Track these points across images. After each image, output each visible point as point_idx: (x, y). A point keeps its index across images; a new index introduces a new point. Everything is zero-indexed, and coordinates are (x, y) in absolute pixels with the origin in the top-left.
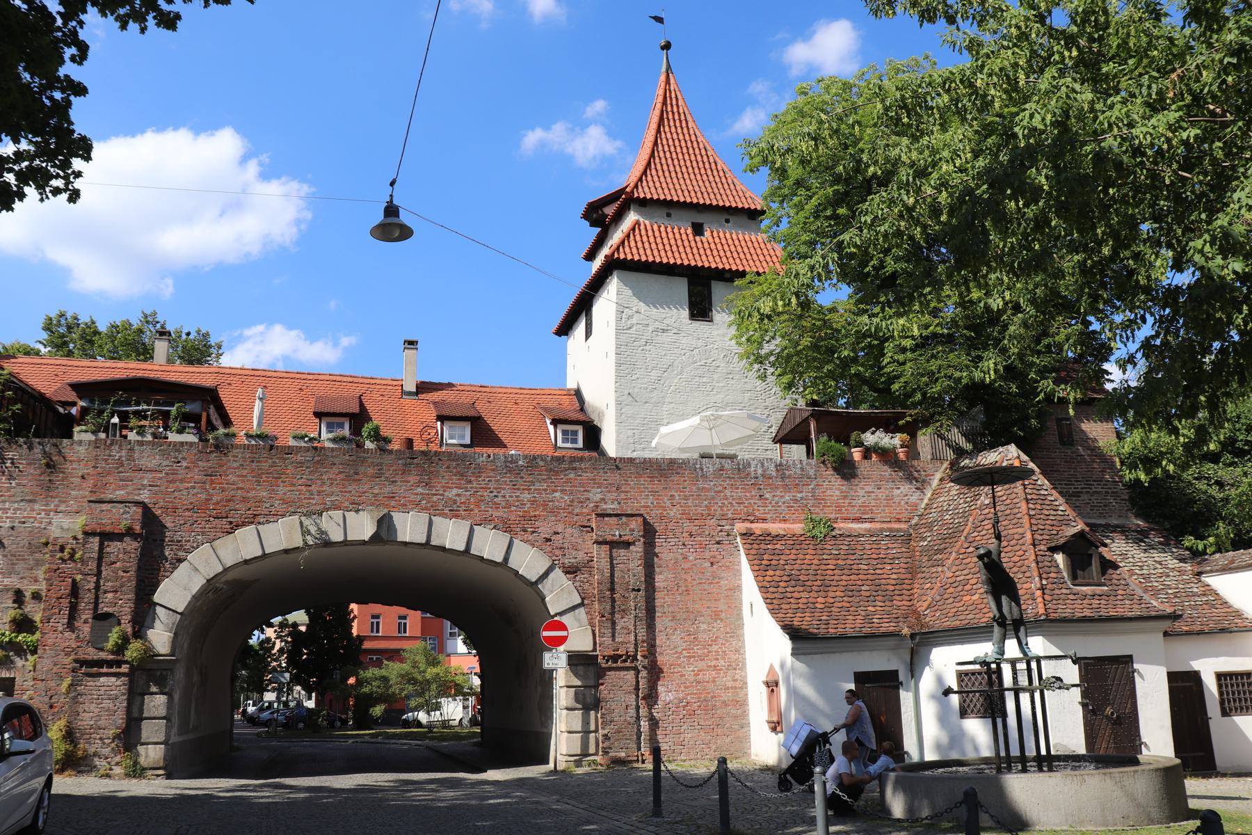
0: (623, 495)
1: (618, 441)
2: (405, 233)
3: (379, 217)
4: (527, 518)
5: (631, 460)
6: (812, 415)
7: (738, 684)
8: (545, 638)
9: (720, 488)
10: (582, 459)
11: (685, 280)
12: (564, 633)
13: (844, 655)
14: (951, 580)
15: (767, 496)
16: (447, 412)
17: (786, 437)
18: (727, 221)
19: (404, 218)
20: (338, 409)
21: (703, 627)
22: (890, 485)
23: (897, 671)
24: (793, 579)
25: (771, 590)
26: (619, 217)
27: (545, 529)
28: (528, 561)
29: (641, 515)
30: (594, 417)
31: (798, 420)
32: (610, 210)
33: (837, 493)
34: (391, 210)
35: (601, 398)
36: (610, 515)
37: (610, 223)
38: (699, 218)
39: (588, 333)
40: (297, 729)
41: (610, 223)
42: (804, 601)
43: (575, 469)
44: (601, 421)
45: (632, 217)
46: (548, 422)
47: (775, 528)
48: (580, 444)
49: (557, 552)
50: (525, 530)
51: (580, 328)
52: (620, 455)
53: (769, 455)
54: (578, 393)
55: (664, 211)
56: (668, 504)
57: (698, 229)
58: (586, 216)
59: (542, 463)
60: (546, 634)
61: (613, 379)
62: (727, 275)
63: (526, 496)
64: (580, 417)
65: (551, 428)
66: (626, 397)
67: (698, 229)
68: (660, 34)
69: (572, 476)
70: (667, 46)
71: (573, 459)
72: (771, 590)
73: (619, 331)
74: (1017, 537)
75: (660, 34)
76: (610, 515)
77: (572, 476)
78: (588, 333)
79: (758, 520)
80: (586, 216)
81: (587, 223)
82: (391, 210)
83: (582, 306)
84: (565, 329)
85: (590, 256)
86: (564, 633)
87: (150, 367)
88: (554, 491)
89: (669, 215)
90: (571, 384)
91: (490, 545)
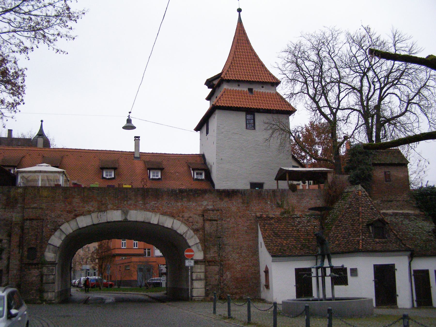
2: (133, 128)
3: (125, 123)
7: (256, 272)
8: (186, 255)
12: (192, 253)
13: (345, 258)
14: (333, 235)
16: (150, 166)
18: (263, 87)
19: (134, 123)
20: (110, 166)
21: (244, 251)
22: (316, 198)
23: (374, 265)
24: (277, 235)
25: (267, 238)
26: (219, 85)
27: (186, 215)
28: (180, 228)
30: (209, 167)
32: (216, 82)
34: (129, 121)
36: (210, 210)
38: (251, 87)
39: (207, 133)
40: (26, 311)
41: (216, 87)
42: (279, 242)
44: (211, 168)
49: (191, 224)
50: (179, 216)
55: (237, 84)
60: (186, 253)
62: (261, 110)
65: (192, 172)
70: (239, 10)
72: (267, 238)
74: (356, 220)
76: (210, 210)
78: (207, 133)
82: (129, 121)
86: (192, 253)
87: (36, 149)
89: (239, 86)
91: (168, 222)
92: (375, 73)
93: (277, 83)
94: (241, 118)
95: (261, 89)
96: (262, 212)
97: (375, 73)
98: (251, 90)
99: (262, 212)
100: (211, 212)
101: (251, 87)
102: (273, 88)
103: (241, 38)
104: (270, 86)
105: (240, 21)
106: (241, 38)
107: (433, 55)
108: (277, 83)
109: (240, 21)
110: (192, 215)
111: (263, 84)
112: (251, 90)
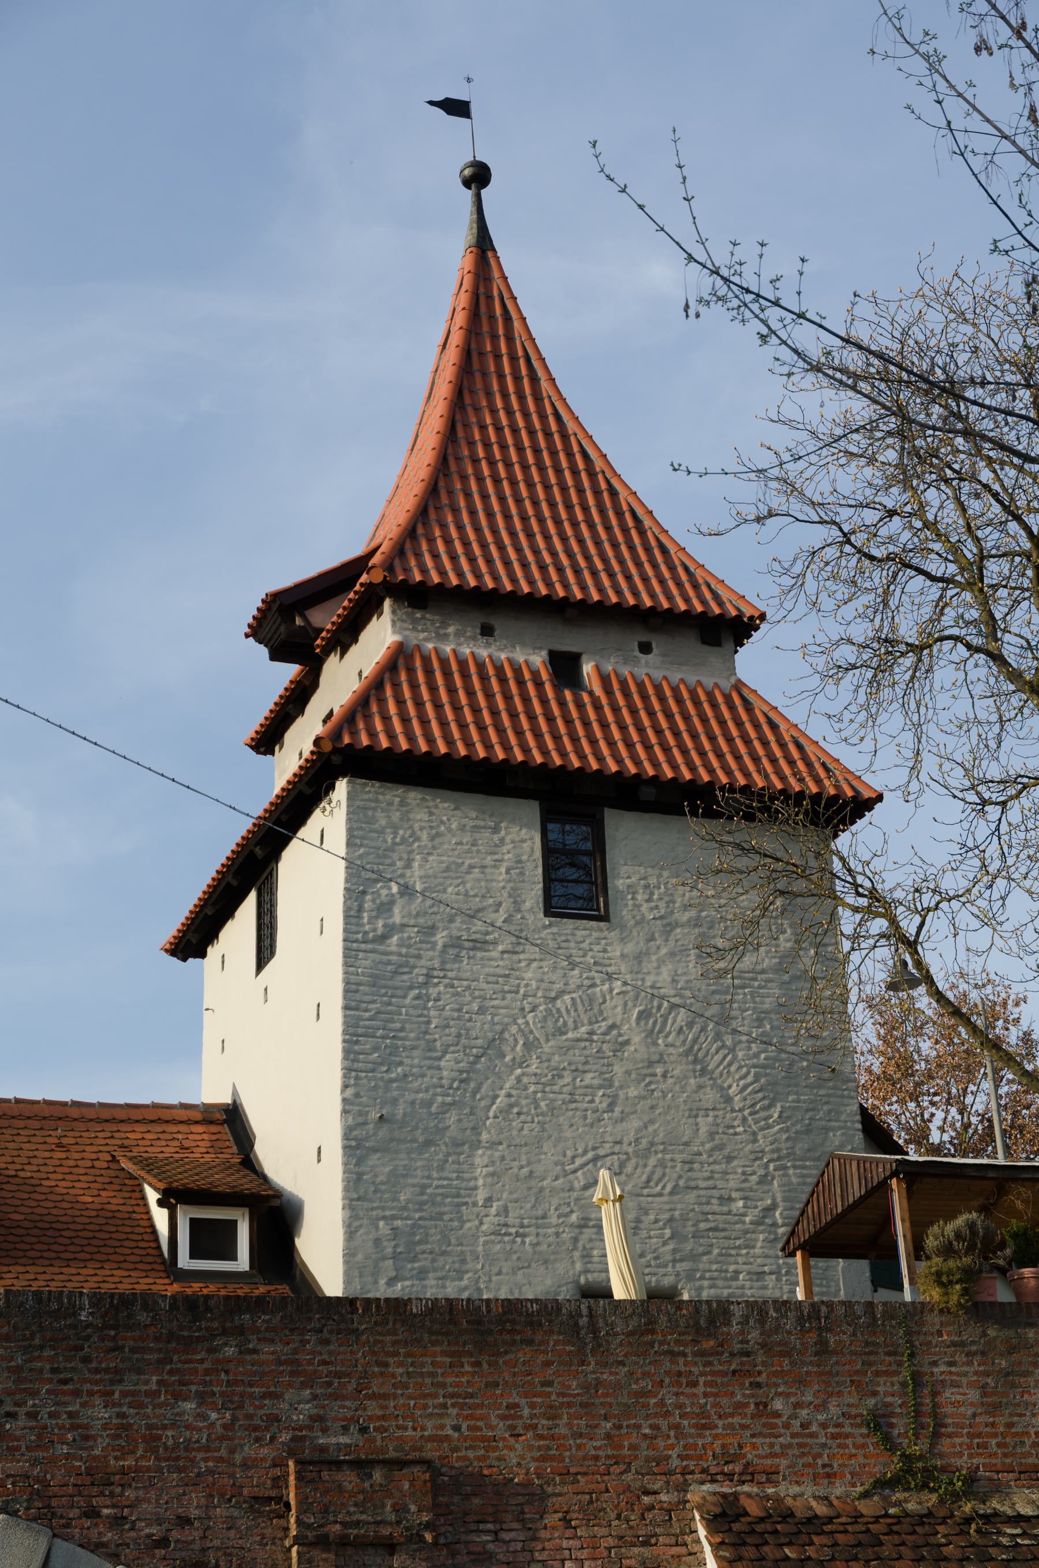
0: (373, 1408)
1: (349, 1255)
2: (978, 50)
4: (100, 1478)
5: (397, 1306)
6: (895, 1174)
9: (647, 1384)
10: (260, 1304)
11: (531, 810)
15: (778, 1405)
17: (823, 1240)
18: (645, 648)
29: (427, 1463)
31: (856, 1191)
33: (974, 1395)
35: (303, 1150)
36: (338, 1464)
37: (327, 651)
43: (240, 1331)
45: (380, 636)
46: (152, 1196)
47: (801, 1495)
48: (243, 1262)
50: (92, 1513)
51: (241, 928)
52: (356, 1291)
53: (772, 1290)
54: (231, 1119)
56: (501, 1428)
57: (576, 887)
58: (257, 631)
59: (143, 1318)
61: (338, 1054)
62: (648, 794)
63: (100, 1414)
64: (246, 1183)
66: (370, 1137)
67: (576, 887)
68: (455, 144)
69: (230, 1351)
71: (235, 1305)
73: (356, 942)
75: (455, 144)
76: (338, 1464)
77: (230, 1351)
79: (749, 1474)
80: (257, 631)
81: (263, 651)
83: (250, 870)
84: (194, 940)
85: (268, 739)
88: (178, 1396)
90: (214, 1093)
92: (840, 438)
93: (733, 629)
94: (516, 842)
95: (636, 661)
96: (730, 1476)
97: (840, 438)
98: (565, 668)
99: (730, 1476)
100: (349, 1479)
101: (568, 643)
102: (713, 656)
103: (488, 341)
104: (690, 644)
105: (483, 244)
106: (488, 341)
107: (318, 691)
108: (733, 629)
109: (483, 244)
110: (194, 1505)
111: (649, 623)
112: (565, 668)
